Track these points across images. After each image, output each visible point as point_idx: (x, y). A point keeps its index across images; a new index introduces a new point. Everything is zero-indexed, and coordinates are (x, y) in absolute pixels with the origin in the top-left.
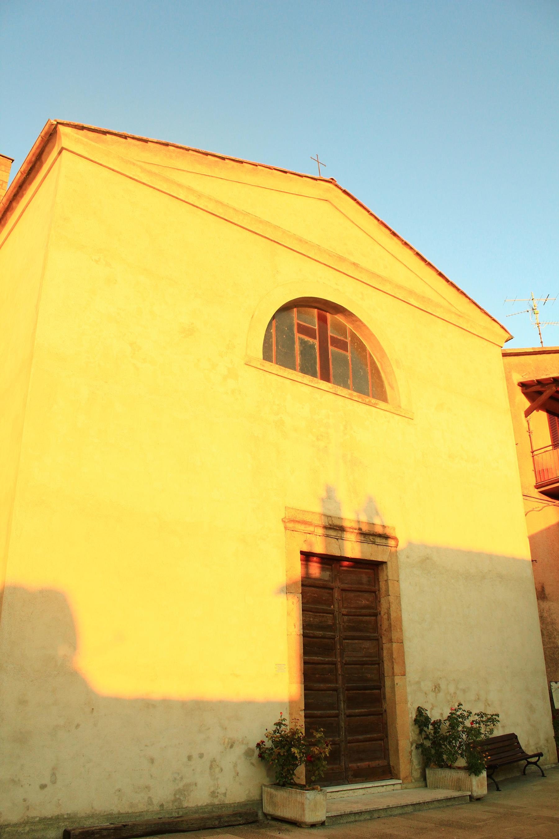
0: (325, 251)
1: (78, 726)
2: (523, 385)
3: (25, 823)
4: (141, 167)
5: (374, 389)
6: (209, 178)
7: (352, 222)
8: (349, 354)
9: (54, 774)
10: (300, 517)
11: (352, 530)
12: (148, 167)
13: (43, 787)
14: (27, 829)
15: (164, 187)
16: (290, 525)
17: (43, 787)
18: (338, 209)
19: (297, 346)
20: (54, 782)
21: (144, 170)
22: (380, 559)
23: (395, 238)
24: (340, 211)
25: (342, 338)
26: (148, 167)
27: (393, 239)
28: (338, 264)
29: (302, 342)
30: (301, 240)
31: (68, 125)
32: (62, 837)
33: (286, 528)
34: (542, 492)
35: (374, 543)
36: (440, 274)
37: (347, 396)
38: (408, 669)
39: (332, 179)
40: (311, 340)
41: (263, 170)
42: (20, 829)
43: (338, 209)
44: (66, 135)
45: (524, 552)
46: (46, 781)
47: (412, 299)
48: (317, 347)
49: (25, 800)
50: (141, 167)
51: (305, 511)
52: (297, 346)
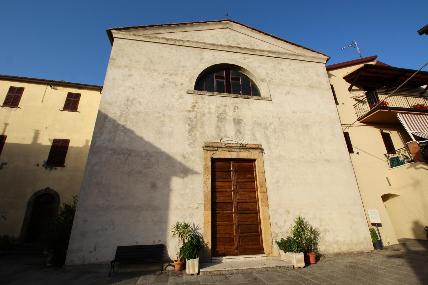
1: (106, 229)
2: (344, 78)
10: (211, 145)
12: (147, 35)
13: (91, 252)
15: (158, 41)
16: (205, 148)
17: (91, 252)
21: (144, 37)
22: (253, 158)
26: (147, 35)
28: (230, 49)
33: (204, 150)
34: (361, 122)
35: (249, 151)
38: (270, 204)
44: (114, 33)
45: (50, 144)
48: (225, 82)
49: (83, 257)
51: (212, 143)
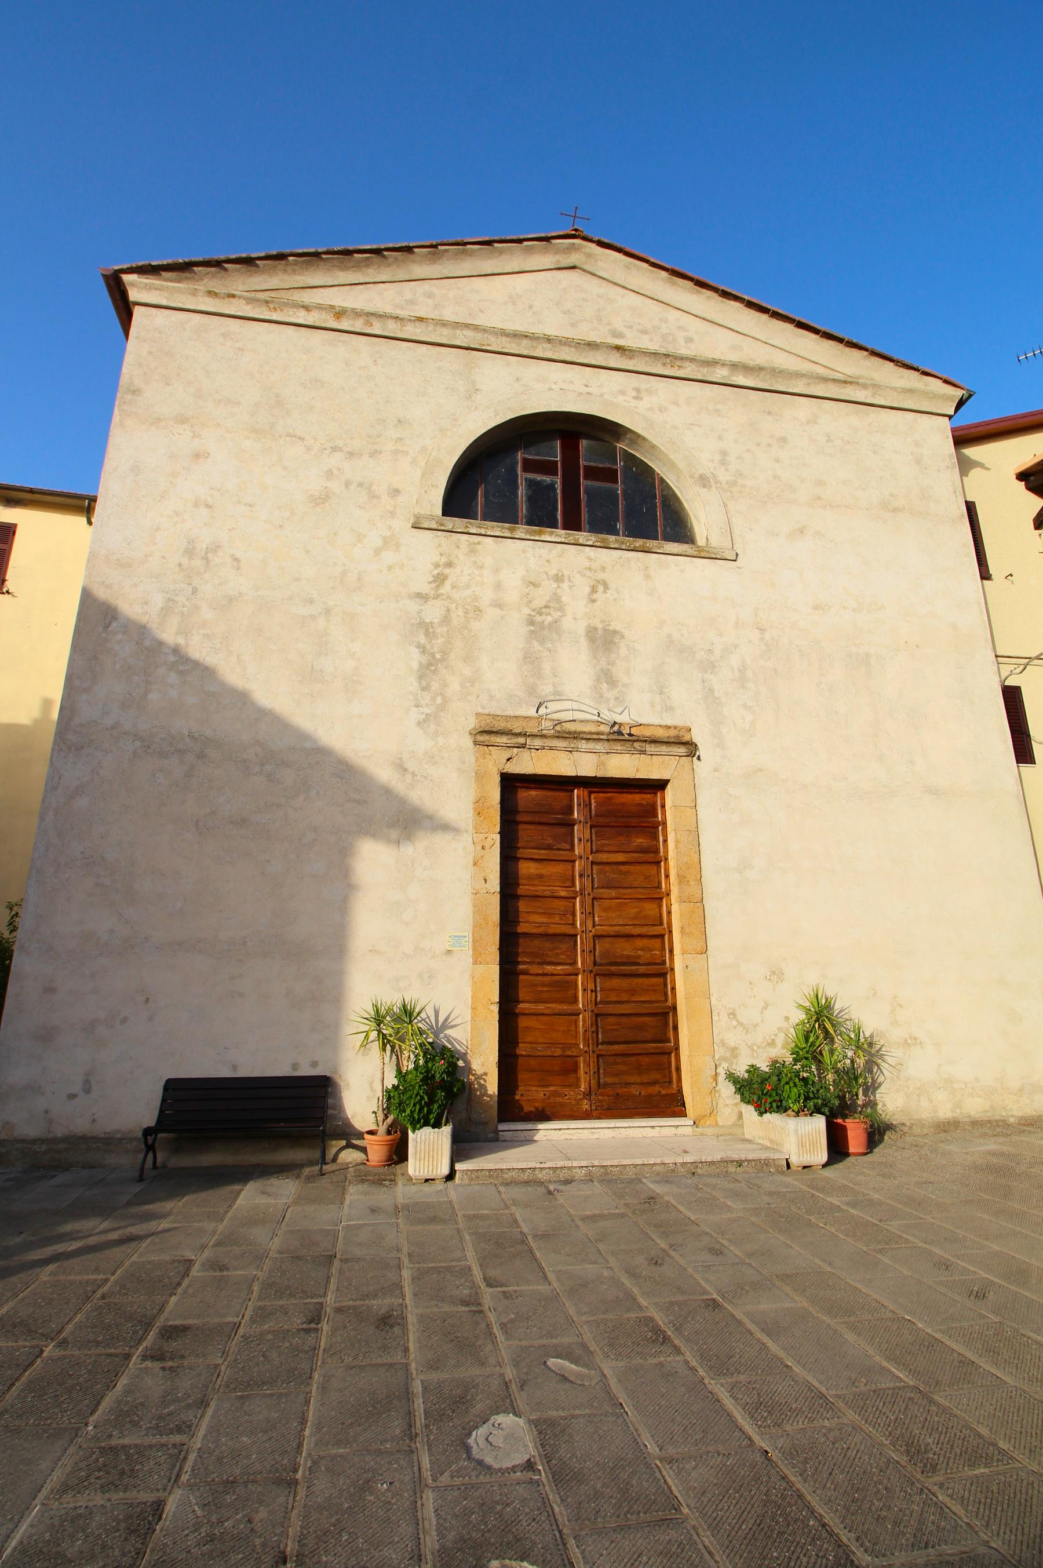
0: (560, 341)
1: (124, 1020)
2: (1022, 476)
3: (42, 1141)
4: (245, 298)
5: (668, 529)
6: (361, 287)
7: (623, 287)
8: (619, 488)
9: (87, 1082)
10: (502, 725)
11: (602, 737)
13: (72, 1096)
14: (44, 1147)
16: (480, 738)
18: (595, 275)
19: (522, 491)
20: (87, 1091)
21: (250, 301)
23: (680, 281)
24: (600, 277)
25: (608, 465)
27: (701, 293)
29: (531, 483)
30: (516, 335)
31: (131, 271)
32: (25, 1122)
33: (476, 743)
36: (801, 325)
37: (598, 544)
39: (576, 230)
40: (547, 479)
41: (446, 251)
42: (35, 1147)
43: (595, 275)
44: (132, 284)
46: (77, 1088)
47: (741, 377)
50: (245, 298)
52: (522, 491)
